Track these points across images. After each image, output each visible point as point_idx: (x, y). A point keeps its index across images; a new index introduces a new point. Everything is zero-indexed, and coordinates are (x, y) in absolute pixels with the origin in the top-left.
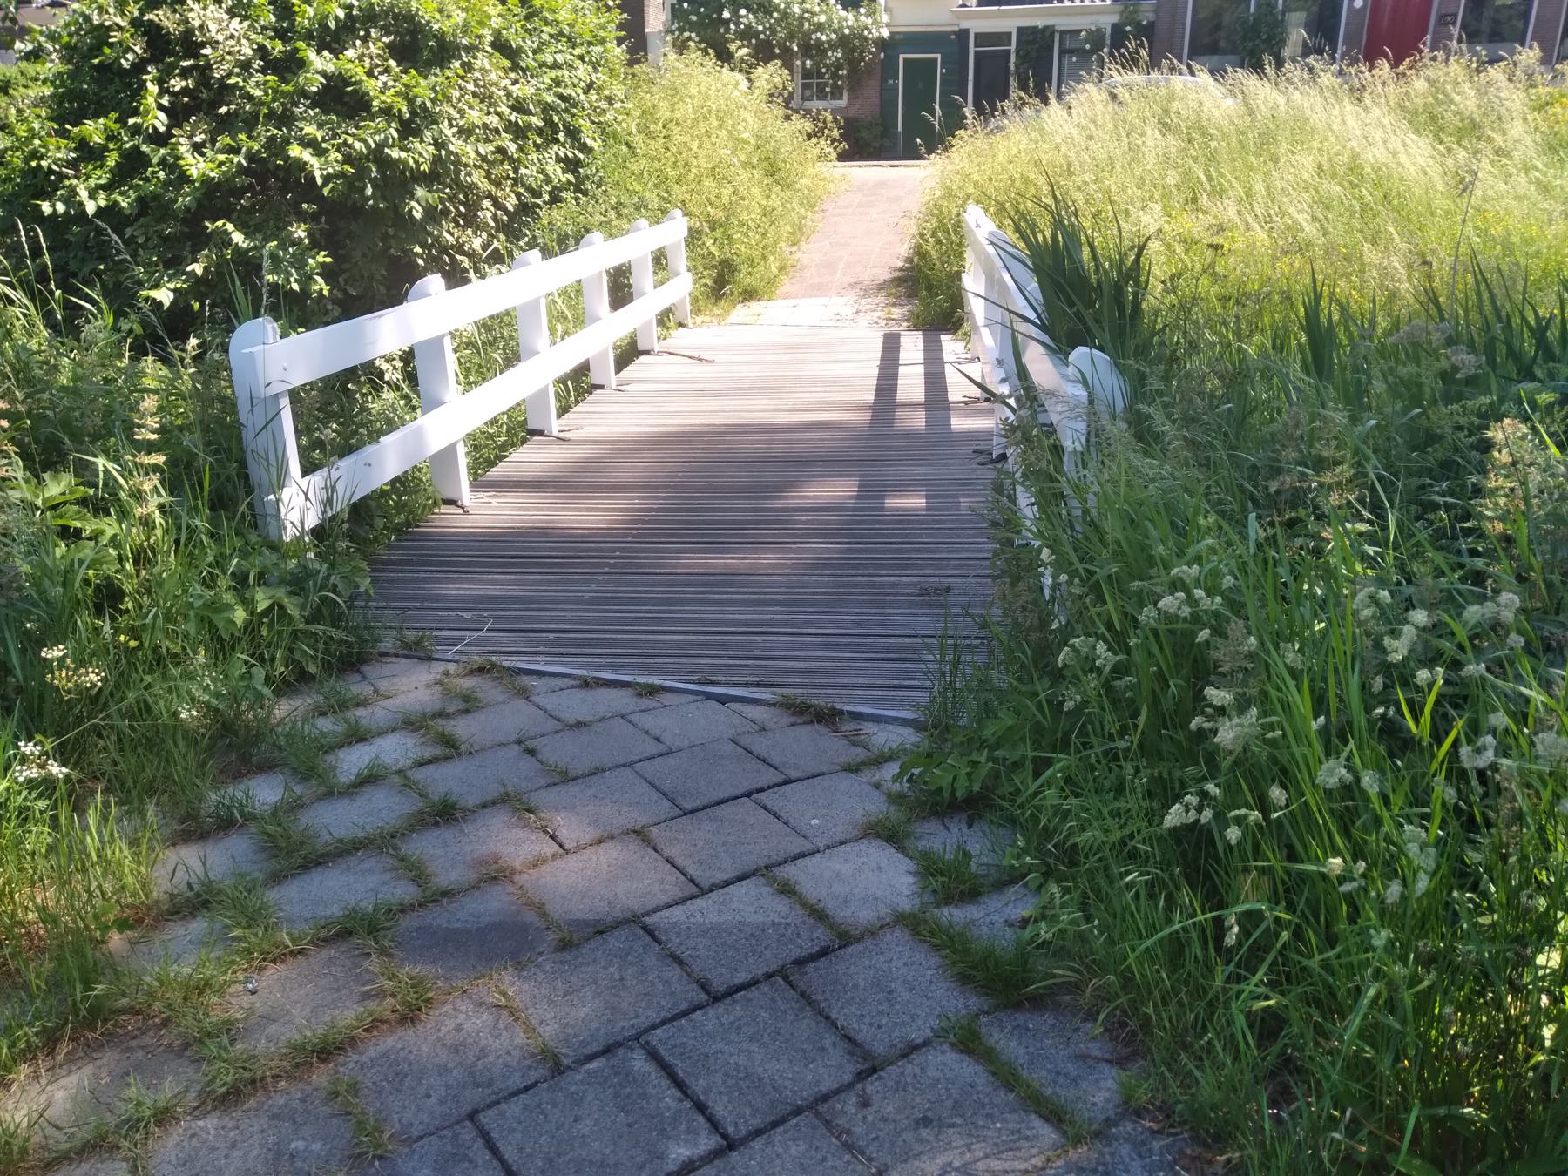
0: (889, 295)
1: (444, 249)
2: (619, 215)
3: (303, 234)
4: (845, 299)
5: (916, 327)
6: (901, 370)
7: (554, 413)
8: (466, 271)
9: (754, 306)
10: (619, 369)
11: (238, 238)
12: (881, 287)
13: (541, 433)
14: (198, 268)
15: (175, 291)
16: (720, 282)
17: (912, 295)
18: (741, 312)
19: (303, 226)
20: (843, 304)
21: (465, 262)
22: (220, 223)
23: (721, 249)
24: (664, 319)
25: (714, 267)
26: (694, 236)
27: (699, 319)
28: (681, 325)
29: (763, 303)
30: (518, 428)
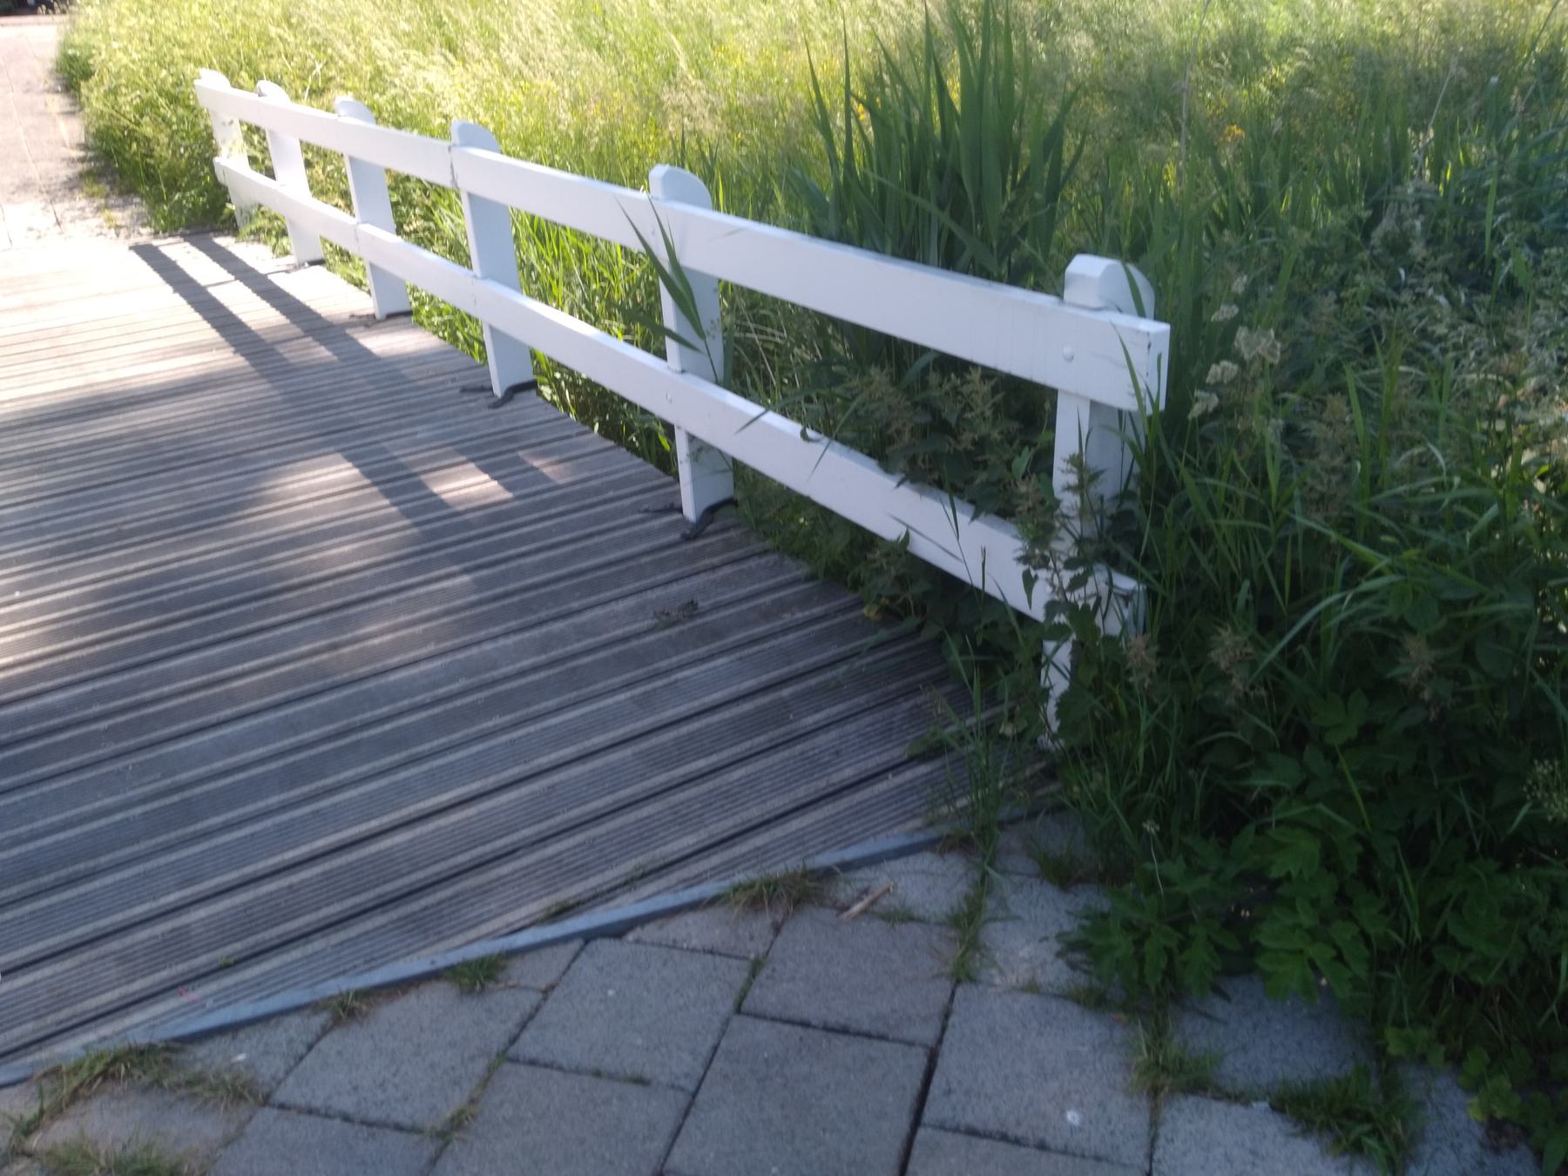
12: (72, 185)
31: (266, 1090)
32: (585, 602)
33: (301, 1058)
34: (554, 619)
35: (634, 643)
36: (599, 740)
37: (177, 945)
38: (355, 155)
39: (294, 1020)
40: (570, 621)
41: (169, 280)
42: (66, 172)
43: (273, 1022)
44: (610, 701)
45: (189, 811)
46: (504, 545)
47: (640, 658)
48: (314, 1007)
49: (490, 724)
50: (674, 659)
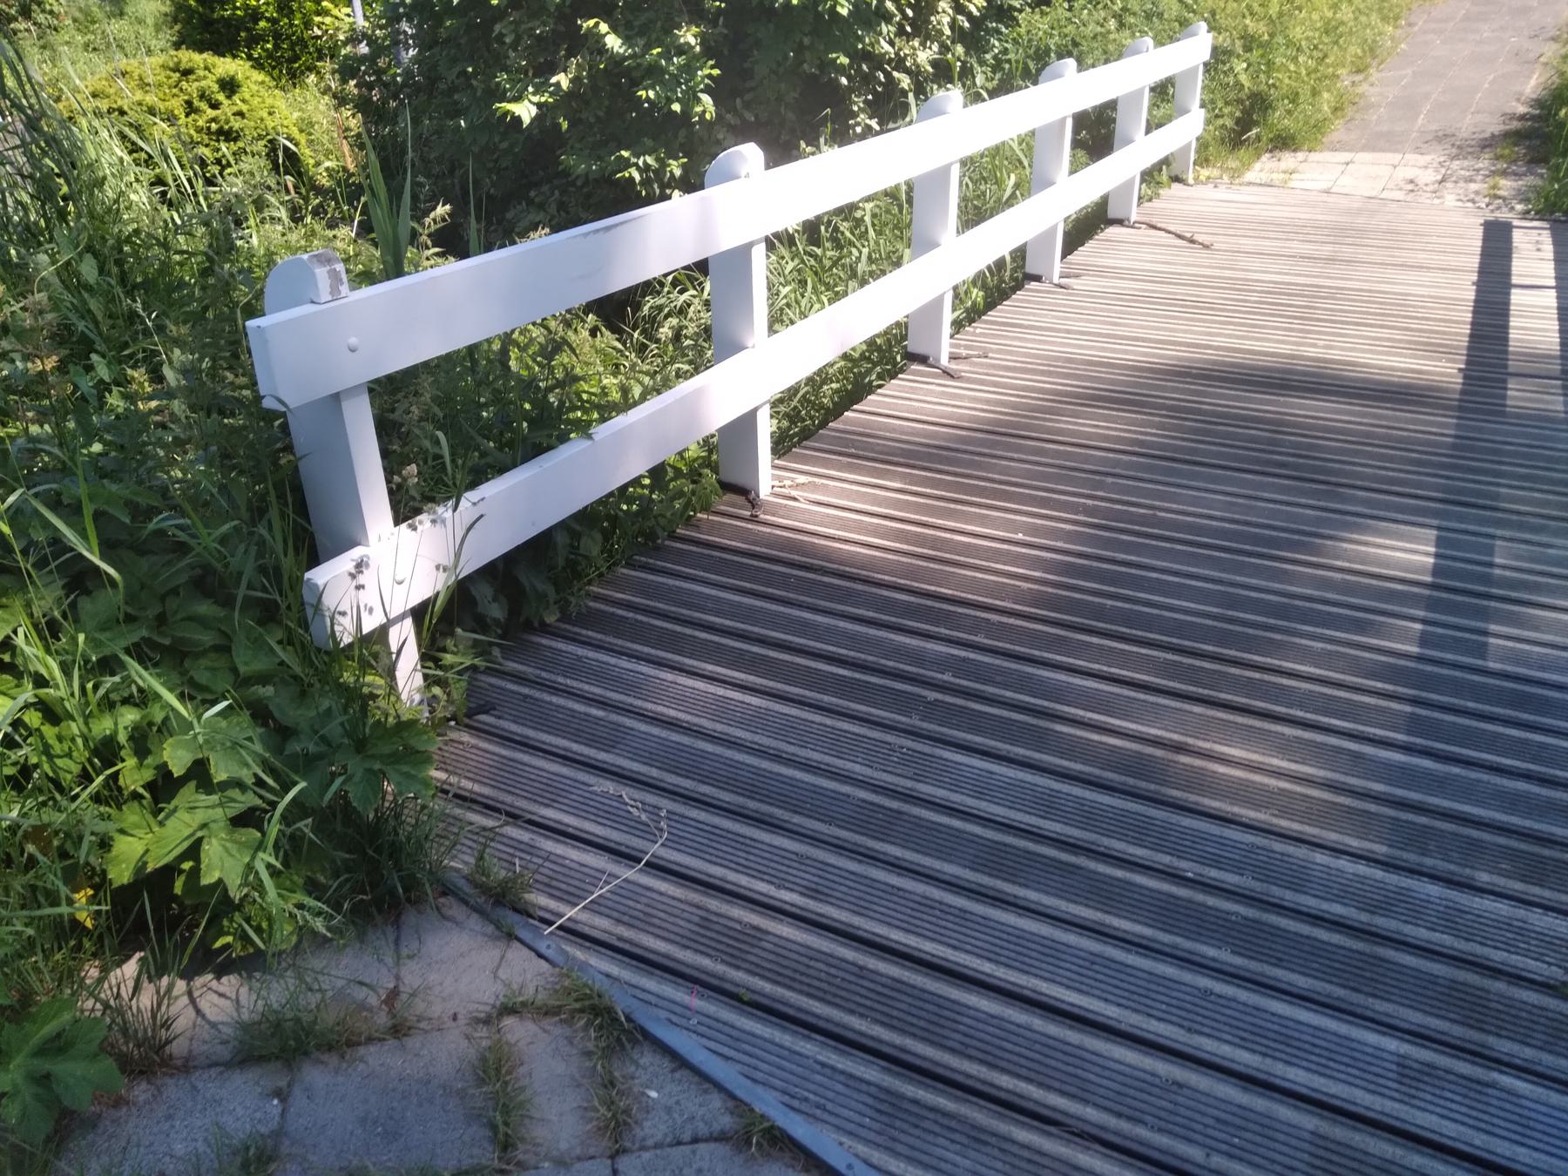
0: (1497, 158)
1: (877, 61)
2: (1121, 25)
3: (692, 41)
4: (1428, 158)
5: (1541, 215)
6: (1516, 297)
7: (947, 329)
8: (904, 93)
9: (1288, 160)
10: (1069, 248)
11: (613, 42)
12: (1487, 144)
13: (923, 359)
14: (563, 80)
15: (539, 105)
16: (1245, 124)
17: (1536, 160)
18: (1265, 167)
19: (694, 29)
20: (1422, 167)
21: (905, 81)
22: (591, 23)
23: (1254, 78)
24: (1150, 176)
25: (1239, 101)
26: (1220, 56)
27: (1205, 173)
28: (1177, 179)
29: (1300, 155)
30: (891, 354)
31: (628, 1144)
32: (1502, 882)
33: (679, 1143)
34: (1434, 878)
35: (1499, 986)
36: (1297, 1077)
37: (738, 946)
38: (981, 105)
39: (716, 1101)
40: (1453, 894)
41: (1483, 270)
42: (1496, 127)
43: (707, 1085)
44: (1372, 1038)
45: (888, 825)
46: (1492, 743)
47: (1474, 1009)
48: (738, 1105)
49: (1211, 952)
50: (1528, 1053)
